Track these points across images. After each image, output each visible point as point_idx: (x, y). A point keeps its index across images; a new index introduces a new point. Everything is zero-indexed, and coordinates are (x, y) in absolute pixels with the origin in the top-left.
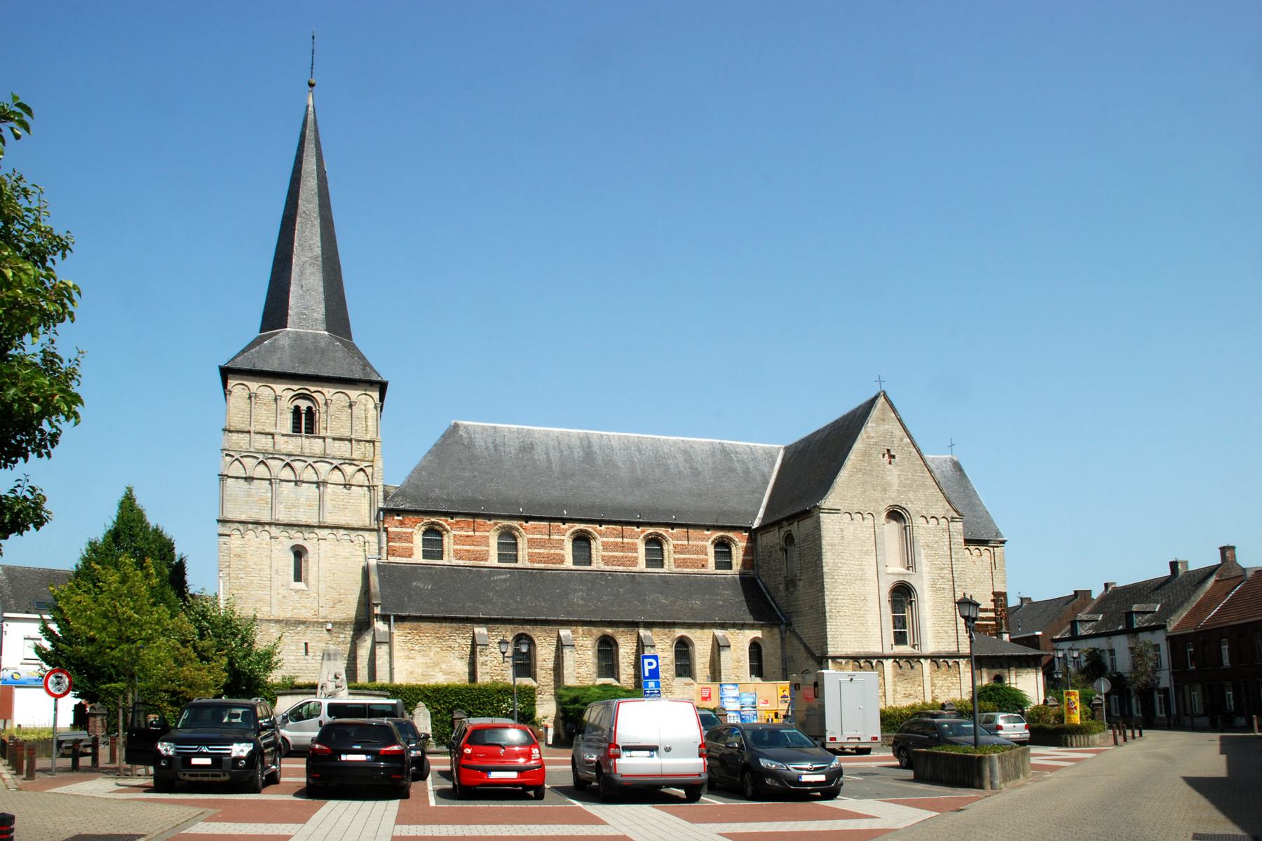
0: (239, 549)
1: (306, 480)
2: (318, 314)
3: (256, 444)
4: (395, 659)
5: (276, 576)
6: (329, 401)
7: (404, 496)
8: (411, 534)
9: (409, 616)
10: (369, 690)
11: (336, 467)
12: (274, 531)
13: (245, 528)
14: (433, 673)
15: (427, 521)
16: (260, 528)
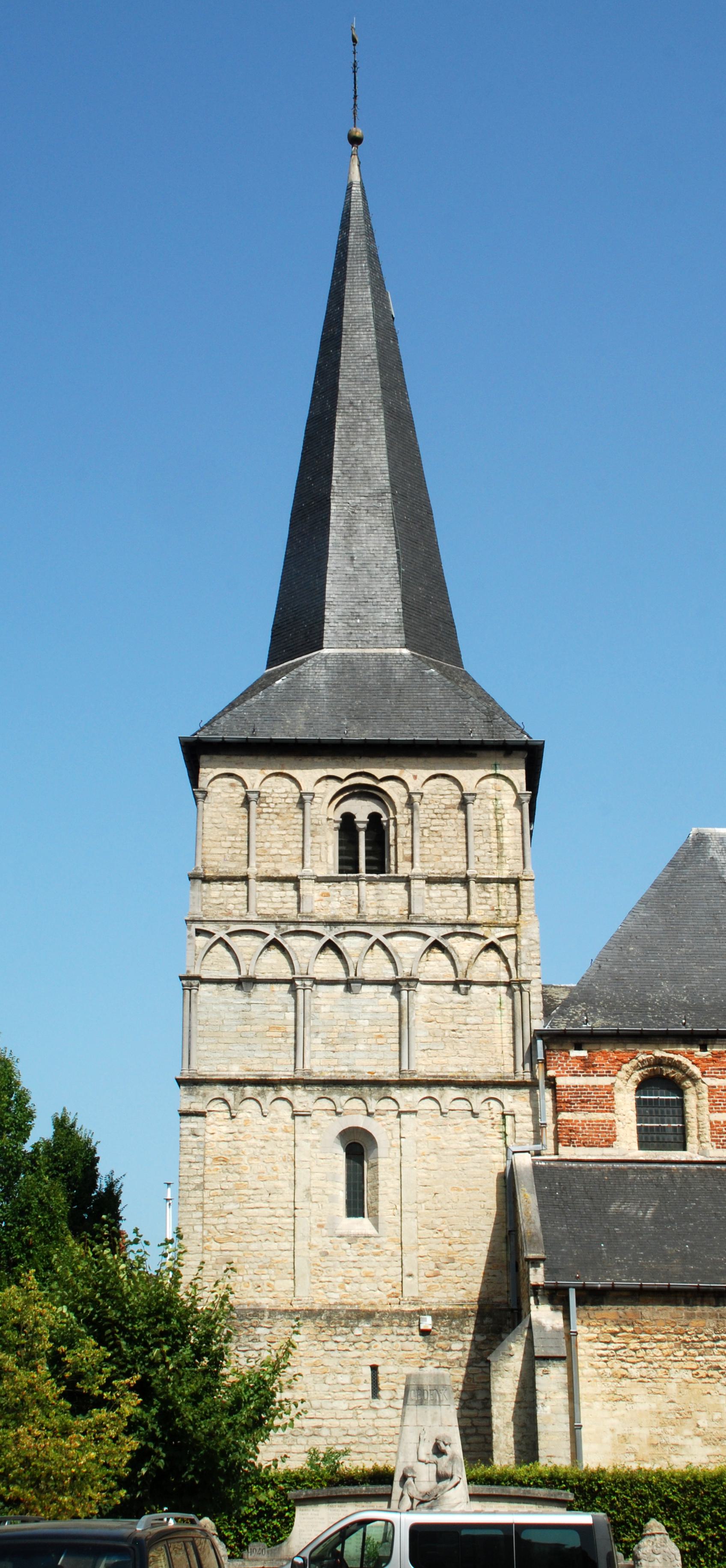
0: (224, 1145)
1: (369, 977)
2: (388, 614)
3: (260, 905)
4: (583, 1403)
5: (306, 1205)
6: (416, 798)
7: (590, 1002)
8: (610, 1089)
9: (613, 1289)
10: (521, 1484)
11: (436, 945)
12: (302, 1098)
13: (239, 1093)
14: (678, 1439)
15: (644, 1057)
16: (271, 1093)
